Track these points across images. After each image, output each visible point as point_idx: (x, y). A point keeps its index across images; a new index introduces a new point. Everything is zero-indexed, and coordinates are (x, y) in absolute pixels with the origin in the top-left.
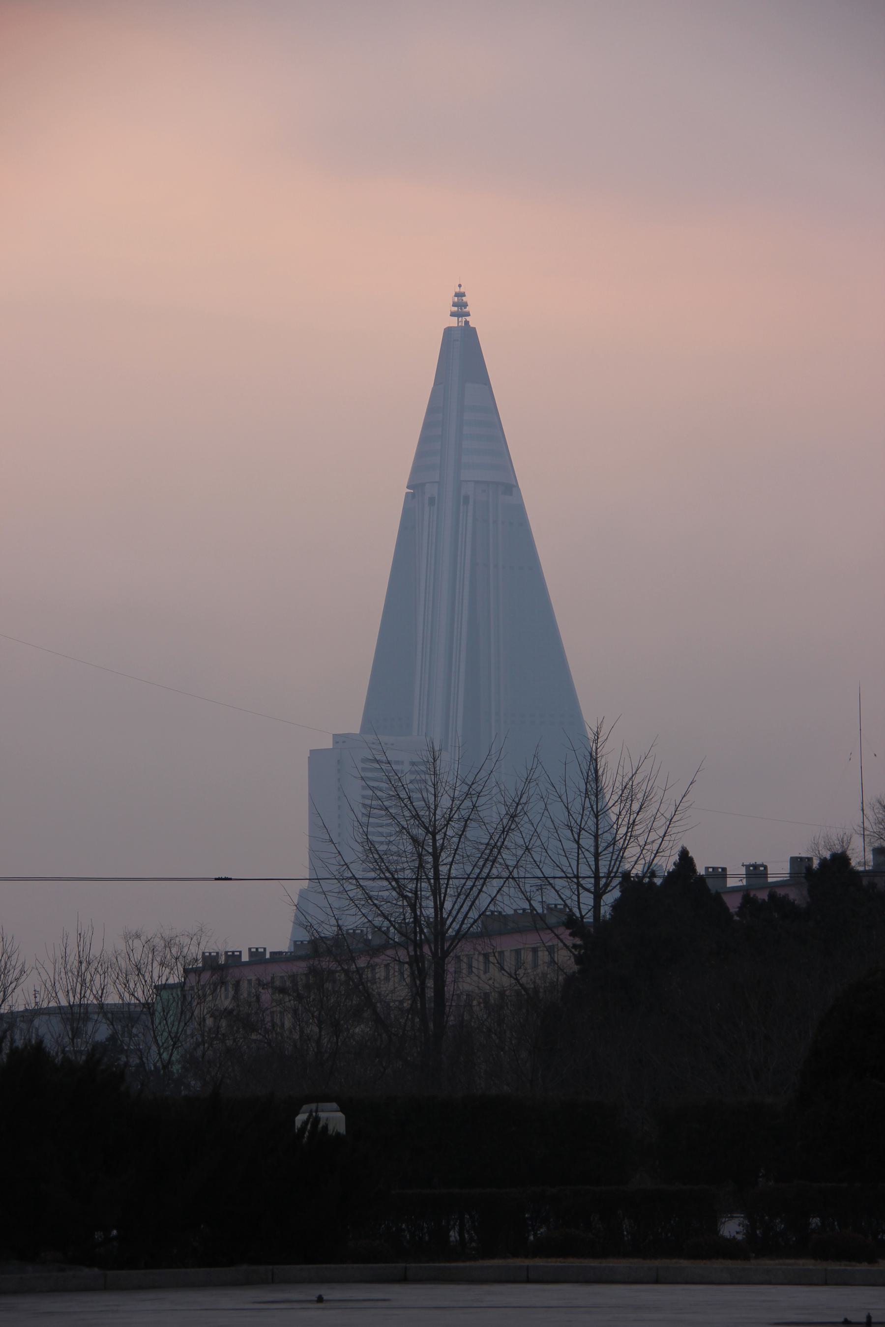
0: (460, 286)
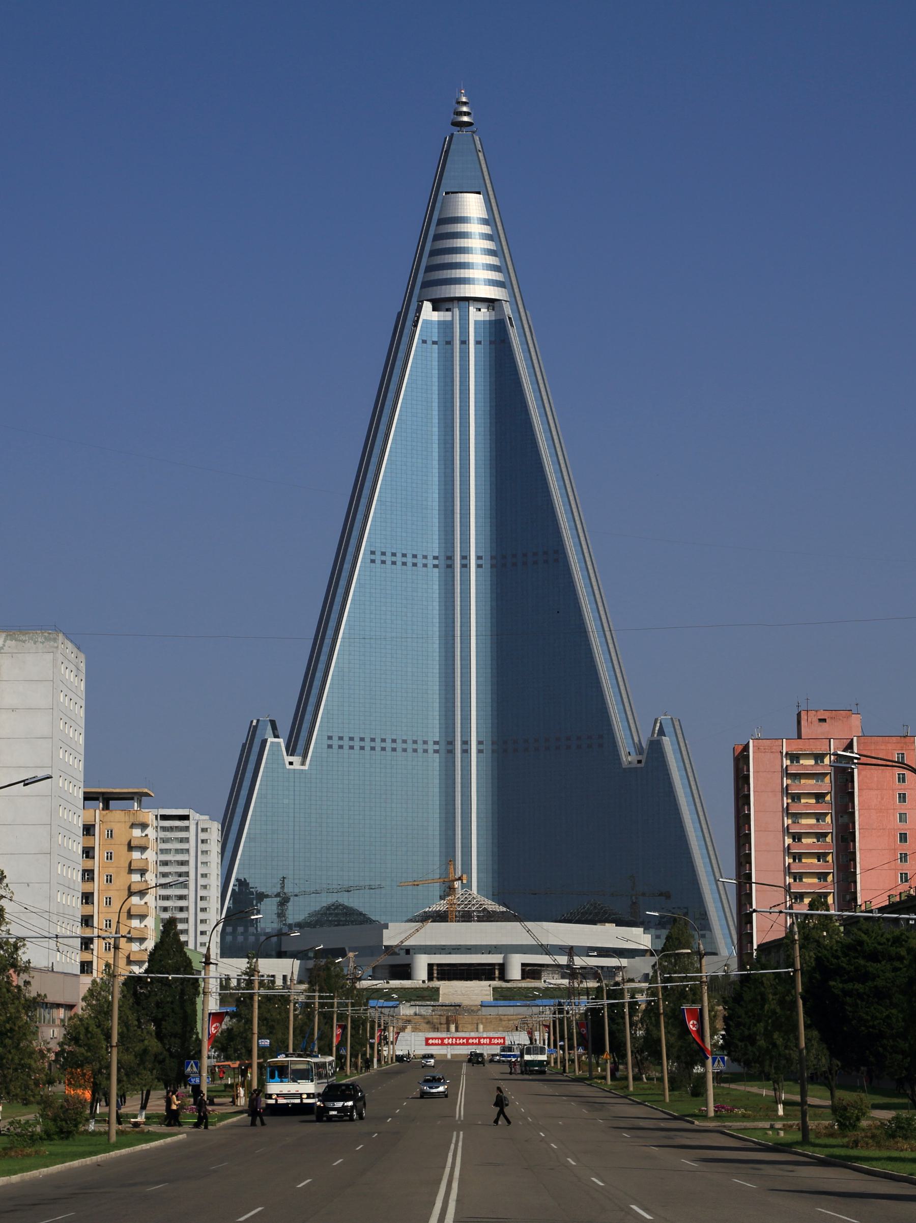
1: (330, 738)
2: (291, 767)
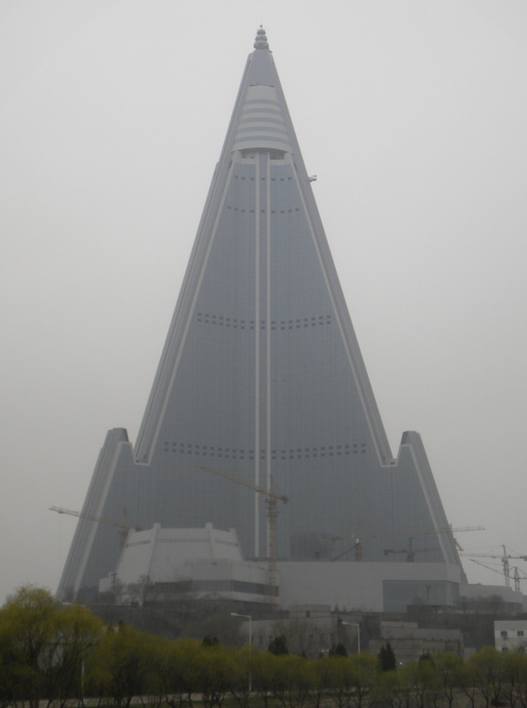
0: (261, 26)
1: (167, 443)
2: (138, 464)
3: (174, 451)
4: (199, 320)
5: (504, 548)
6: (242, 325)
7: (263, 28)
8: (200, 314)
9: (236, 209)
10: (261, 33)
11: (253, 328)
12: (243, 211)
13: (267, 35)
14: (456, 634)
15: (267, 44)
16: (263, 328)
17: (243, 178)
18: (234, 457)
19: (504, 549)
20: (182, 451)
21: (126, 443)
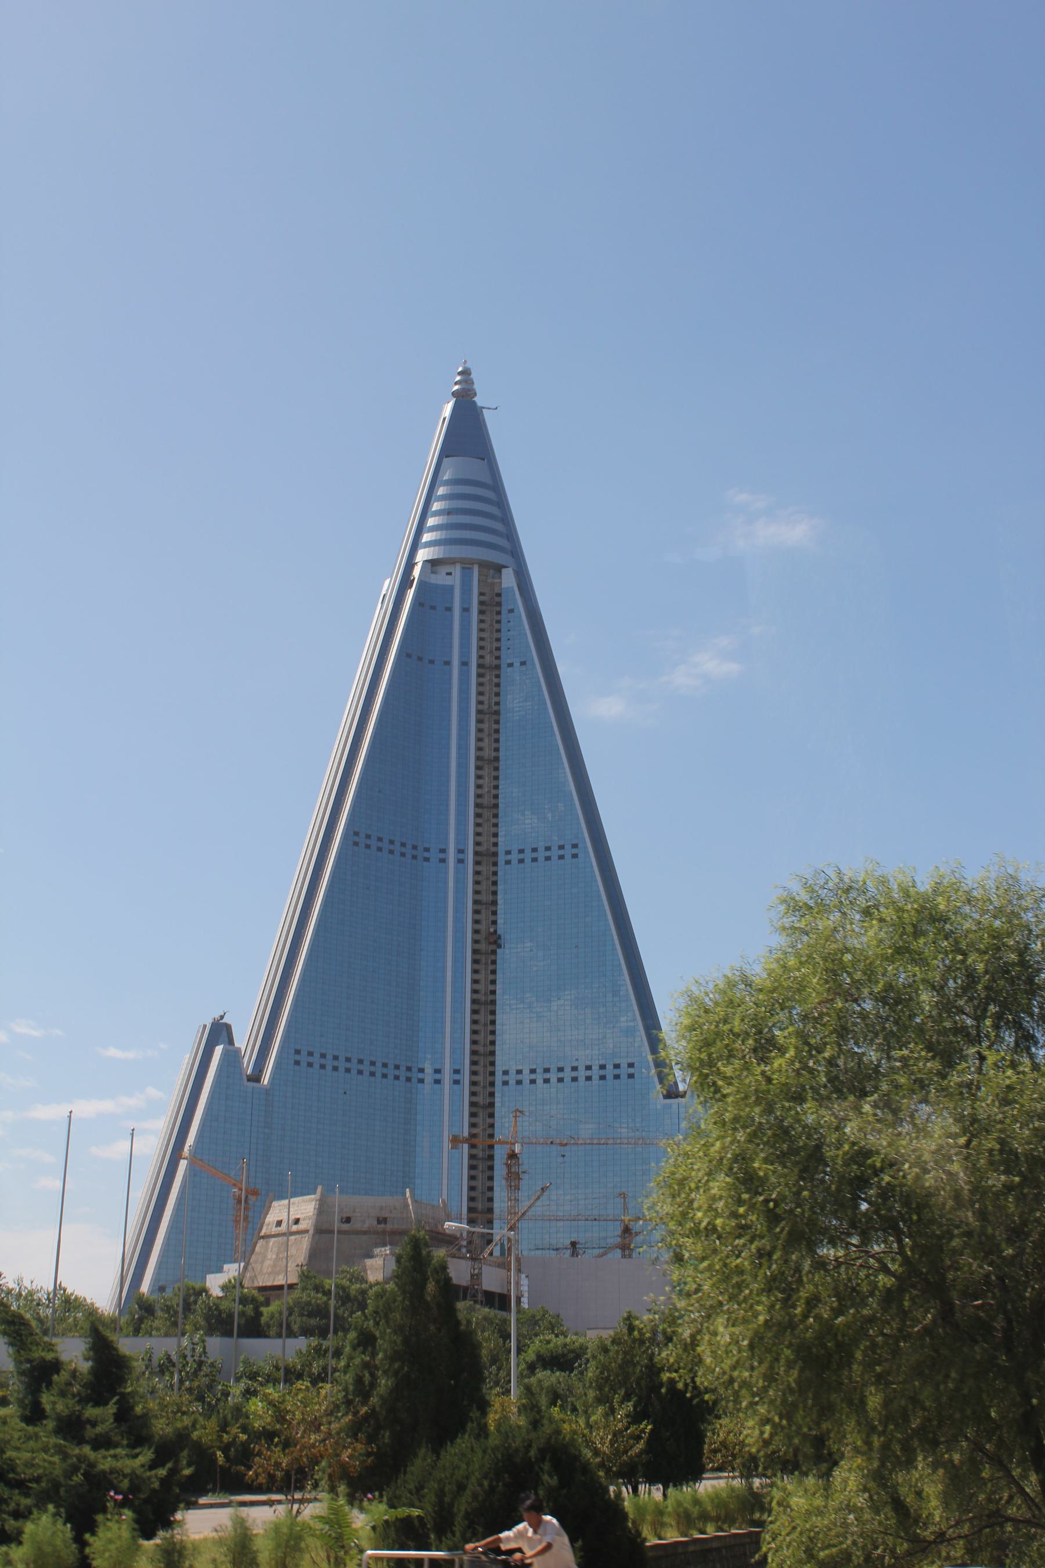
1: (298, 1052)
3: (603, 1078)
4: (356, 844)
5: (624, 1198)
6: (426, 854)
7: (467, 365)
8: (356, 834)
9: (420, 659)
10: (466, 373)
11: (443, 861)
12: (432, 662)
13: (474, 376)
14: (219, 1050)
15: (474, 390)
16: (461, 861)
17: (433, 608)
18: (409, 1079)
19: (625, 1201)
20: (310, 1065)
21: (231, 1048)
